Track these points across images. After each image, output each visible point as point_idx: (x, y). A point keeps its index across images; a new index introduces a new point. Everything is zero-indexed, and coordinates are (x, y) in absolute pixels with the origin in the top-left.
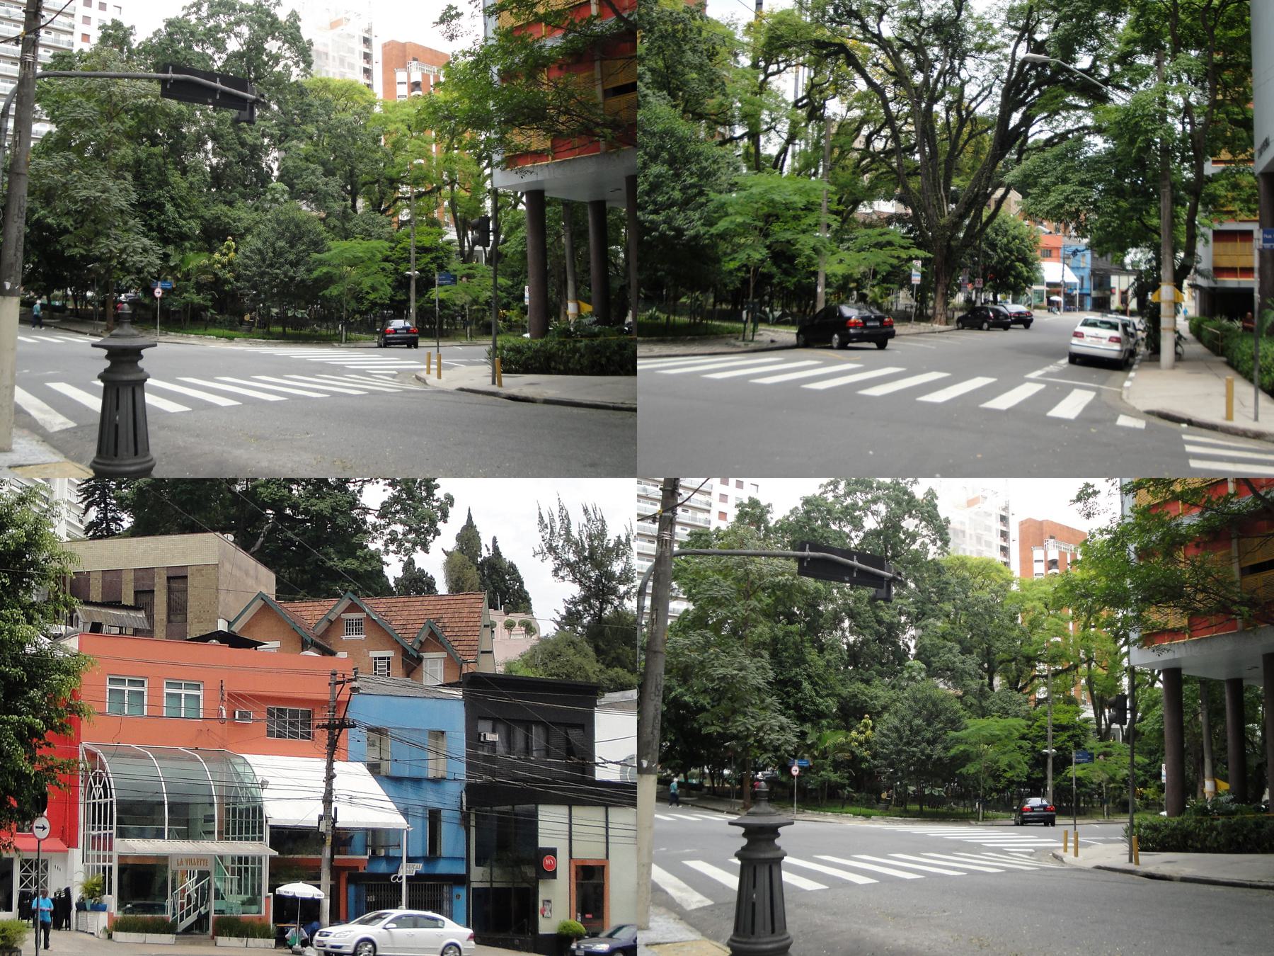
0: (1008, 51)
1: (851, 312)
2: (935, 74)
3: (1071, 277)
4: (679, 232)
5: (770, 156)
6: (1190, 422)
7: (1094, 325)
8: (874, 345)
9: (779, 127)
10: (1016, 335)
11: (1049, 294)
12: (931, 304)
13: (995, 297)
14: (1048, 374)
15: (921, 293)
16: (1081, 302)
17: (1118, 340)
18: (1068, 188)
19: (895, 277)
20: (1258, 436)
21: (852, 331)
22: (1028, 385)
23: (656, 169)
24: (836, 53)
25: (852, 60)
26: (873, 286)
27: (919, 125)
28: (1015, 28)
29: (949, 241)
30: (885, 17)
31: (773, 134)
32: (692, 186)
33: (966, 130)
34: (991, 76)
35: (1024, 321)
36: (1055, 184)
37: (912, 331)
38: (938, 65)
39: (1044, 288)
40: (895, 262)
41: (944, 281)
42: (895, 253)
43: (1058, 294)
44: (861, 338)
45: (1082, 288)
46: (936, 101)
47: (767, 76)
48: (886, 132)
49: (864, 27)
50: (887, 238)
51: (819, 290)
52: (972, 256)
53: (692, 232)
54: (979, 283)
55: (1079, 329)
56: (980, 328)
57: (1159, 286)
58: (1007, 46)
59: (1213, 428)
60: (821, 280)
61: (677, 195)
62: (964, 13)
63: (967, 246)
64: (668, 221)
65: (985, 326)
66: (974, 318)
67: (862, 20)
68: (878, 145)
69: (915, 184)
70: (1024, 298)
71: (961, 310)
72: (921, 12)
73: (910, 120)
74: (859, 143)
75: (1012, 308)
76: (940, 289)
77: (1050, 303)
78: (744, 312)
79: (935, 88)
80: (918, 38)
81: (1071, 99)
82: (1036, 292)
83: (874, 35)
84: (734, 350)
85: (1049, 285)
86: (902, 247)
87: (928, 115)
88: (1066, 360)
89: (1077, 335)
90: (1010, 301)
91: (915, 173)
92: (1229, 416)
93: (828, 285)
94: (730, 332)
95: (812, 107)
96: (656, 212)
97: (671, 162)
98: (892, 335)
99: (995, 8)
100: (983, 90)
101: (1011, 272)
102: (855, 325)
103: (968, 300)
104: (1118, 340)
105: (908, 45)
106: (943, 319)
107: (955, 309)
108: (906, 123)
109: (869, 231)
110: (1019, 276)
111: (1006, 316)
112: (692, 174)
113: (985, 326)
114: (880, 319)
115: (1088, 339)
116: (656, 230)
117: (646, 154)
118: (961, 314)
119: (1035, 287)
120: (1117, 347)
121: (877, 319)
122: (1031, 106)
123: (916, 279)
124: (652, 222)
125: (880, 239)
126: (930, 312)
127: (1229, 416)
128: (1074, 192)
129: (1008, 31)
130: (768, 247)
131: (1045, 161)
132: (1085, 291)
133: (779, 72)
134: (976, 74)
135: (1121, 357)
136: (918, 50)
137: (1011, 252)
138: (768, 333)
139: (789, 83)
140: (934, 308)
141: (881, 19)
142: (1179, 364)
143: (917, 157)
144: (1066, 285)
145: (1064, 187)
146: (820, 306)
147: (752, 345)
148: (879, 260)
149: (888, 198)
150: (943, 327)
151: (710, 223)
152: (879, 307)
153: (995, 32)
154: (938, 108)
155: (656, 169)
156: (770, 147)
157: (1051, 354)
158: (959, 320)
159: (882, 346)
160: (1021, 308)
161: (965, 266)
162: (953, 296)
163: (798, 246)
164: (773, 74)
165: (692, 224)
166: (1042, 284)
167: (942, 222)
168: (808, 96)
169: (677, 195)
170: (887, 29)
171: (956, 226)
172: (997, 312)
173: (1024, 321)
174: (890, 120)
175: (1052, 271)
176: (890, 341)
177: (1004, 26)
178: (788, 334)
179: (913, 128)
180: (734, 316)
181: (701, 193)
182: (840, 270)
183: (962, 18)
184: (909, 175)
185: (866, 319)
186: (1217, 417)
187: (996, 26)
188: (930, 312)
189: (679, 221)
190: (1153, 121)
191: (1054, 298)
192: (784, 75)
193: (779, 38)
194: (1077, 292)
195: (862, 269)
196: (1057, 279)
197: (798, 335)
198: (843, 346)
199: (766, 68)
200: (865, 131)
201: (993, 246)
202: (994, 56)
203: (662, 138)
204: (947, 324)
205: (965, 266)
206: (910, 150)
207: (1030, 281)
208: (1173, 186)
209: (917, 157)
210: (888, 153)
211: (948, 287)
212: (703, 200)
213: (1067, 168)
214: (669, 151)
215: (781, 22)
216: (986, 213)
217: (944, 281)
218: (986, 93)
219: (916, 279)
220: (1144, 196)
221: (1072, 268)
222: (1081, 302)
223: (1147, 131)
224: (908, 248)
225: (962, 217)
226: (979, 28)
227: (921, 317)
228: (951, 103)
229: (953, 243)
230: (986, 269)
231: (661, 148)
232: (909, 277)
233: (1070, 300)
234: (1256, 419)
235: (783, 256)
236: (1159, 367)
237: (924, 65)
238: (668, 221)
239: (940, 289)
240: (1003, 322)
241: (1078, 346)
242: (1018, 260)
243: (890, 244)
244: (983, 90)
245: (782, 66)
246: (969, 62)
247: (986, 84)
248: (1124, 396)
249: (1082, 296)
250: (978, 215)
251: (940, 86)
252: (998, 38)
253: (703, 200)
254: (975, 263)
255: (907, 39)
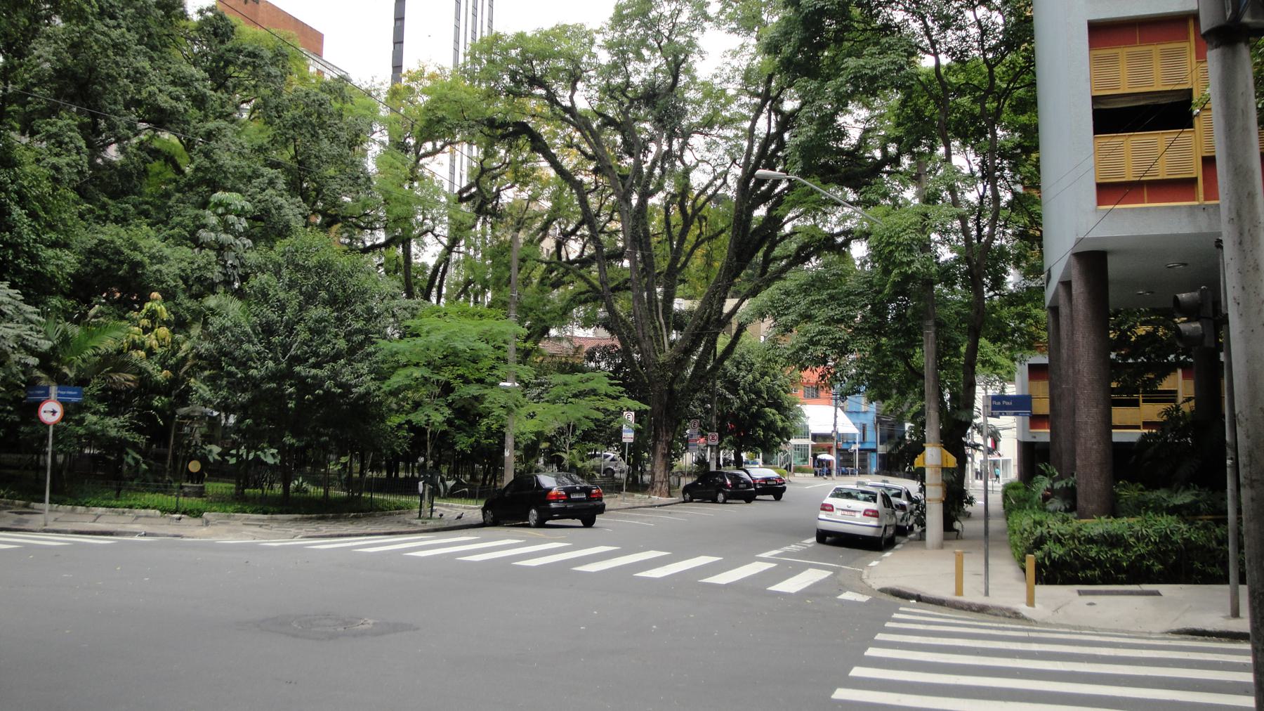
0: (747, 125)
1: (548, 481)
2: (650, 157)
3: (847, 426)
4: (347, 388)
5: (424, 266)
6: (919, 598)
7: (848, 495)
8: (578, 522)
9: (438, 230)
10: (762, 509)
11: (816, 450)
12: (648, 467)
13: (738, 456)
14: (786, 554)
15: (634, 454)
16: (863, 462)
17: (875, 514)
18: (813, 328)
19: (604, 433)
20: (982, 609)
21: (553, 505)
22: (757, 564)
23: (316, 312)
24: (516, 135)
25: (539, 145)
26: (571, 446)
27: (629, 231)
28: (754, 94)
29: (671, 385)
30: (580, 85)
31: (429, 238)
32: (359, 331)
33: (694, 231)
34: (728, 159)
35: (774, 490)
36: (796, 323)
37: (624, 504)
38: (653, 147)
39: (809, 442)
40: (600, 416)
41: (665, 437)
42: (599, 404)
43: (829, 450)
44: (564, 513)
45: (863, 441)
46: (652, 194)
47: (419, 158)
48: (585, 230)
49: (552, 98)
50: (590, 385)
51: (507, 454)
52: (703, 402)
53: (362, 390)
54: (713, 438)
55: (828, 500)
56: (715, 501)
57: (924, 449)
58: (745, 118)
59: (940, 603)
60: (509, 442)
61: (342, 344)
62: (683, 79)
63: (695, 391)
64: (334, 375)
65: (721, 497)
66: (707, 487)
67: (547, 88)
68: (574, 249)
69: (622, 304)
70: (780, 457)
71: (689, 474)
72: (628, 76)
73: (616, 216)
74: (548, 245)
75: (759, 471)
76: (661, 448)
77: (820, 463)
78: (421, 483)
79: (651, 173)
80: (625, 113)
81: (834, 192)
82: (797, 447)
83: (566, 109)
84: (411, 529)
85: (815, 437)
86: (610, 396)
87: (642, 212)
88: (814, 539)
89: (827, 508)
90: (760, 461)
91: (622, 287)
92: (959, 591)
93: (516, 446)
94: (398, 508)
95: (480, 198)
96: (318, 365)
97: (332, 301)
98: (601, 509)
99: (728, 69)
100: (715, 179)
101: (758, 424)
102: (557, 498)
103: (701, 462)
104: (875, 514)
105: (609, 122)
106: (665, 488)
107: (683, 474)
108: (611, 219)
109: (567, 378)
110: (770, 426)
111: (748, 484)
112: (357, 316)
113: (721, 497)
114: (587, 491)
115: (839, 513)
116: (321, 387)
117: (301, 293)
118: (689, 481)
119: (793, 441)
120: (874, 522)
121: (583, 490)
122: (780, 199)
123: (628, 437)
124: (315, 377)
125: (582, 387)
126: (647, 478)
127: (959, 591)
128: (821, 333)
129: (745, 99)
130: (449, 405)
131: (787, 293)
132: (867, 446)
133: (435, 152)
134: (708, 156)
135: (880, 533)
136: (624, 127)
137: (758, 393)
138: (451, 509)
139: (449, 167)
140: (653, 473)
141: (574, 89)
142: (946, 543)
143: (626, 263)
144: (842, 437)
145: (809, 326)
146: (509, 477)
147: (431, 524)
148: (579, 415)
149: (587, 323)
150: (664, 500)
151: (381, 376)
152: (581, 473)
153: (730, 101)
154: (656, 200)
155: (316, 312)
156: (427, 254)
157: (792, 532)
158: (687, 489)
159: (588, 523)
160: (770, 473)
161: (694, 416)
162: (678, 456)
163: (486, 404)
164: (427, 155)
165: (359, 378)
166: (806, 435)
167: (662, 358)
168: (477, 183)
169: (342, 344)
170: (583, 99)
171: (680, 363)
172: (736, 479)
173: (774, 490)
174: (588, 218)
175: (820, 416)
176: (598, 518)
177: (740, 92)
178: (473, 510)
179: (619, 226)
180: (408, 487)
181: (368, 340)
182: (530, 427)
183: (681, 84)
184: (616, 289)
185: (569, 491)
186: (947, 593)
187: (731, 92)
188: (647, 478)
189: (346, 376)
190: (910, 251)
191: (824, 456)
192: (439, 156)
193: (440, 121)
194: (856, 447)
195: (557, 425)
196: (827, 429)
197: (484, 510)
198: (540, 524)
199: (418, 146)
200: (555, 230)
201: (733, 385)
202: (729, 133)
203: (318, 274)
204: (670, 496)
205: (694, 416)
206: (619, 256)
207: (785, 434)
208: (940, 325)
209: (626, 263)
210: (583, 262)
211: (670, 445)
212: (372, 349)
213: (813, 303)
214: (327, 289)
215: (441, 99)
216: (722, 342)
217: (665, 437)
218: (719, 182)
219: (628, 437)
220: (909, 335)
221: (849, 413)
222: (863, 462)
223: (902, 263)
224: (617, 398)
225: (688, 351)
226: (706, 96)
227: (636, 486)
228: (674, 196)
229: (676, 387)
230: (723, 418)
231: (319, 285)
232: (618, 433)
233: (846, 460)
234: (987, 594)
235: (467, 414)
236: (924, 546)
237: (633, 146)
238: (334, 375)
239: (661, 448)
240: (746, 493)
241: (828, 521)
242: (769, 405)
243: (594, 392)
244: (715, 179)
245: (439, 144)
246: (697, 140)
247: (719, 170)
248: (864, 577)
249: (863, 452)
250: (712, 343)
251: (657, 171)
252: (734, 107)
253: (372, 349)
254: (707, 412)
255: (611, 113)
